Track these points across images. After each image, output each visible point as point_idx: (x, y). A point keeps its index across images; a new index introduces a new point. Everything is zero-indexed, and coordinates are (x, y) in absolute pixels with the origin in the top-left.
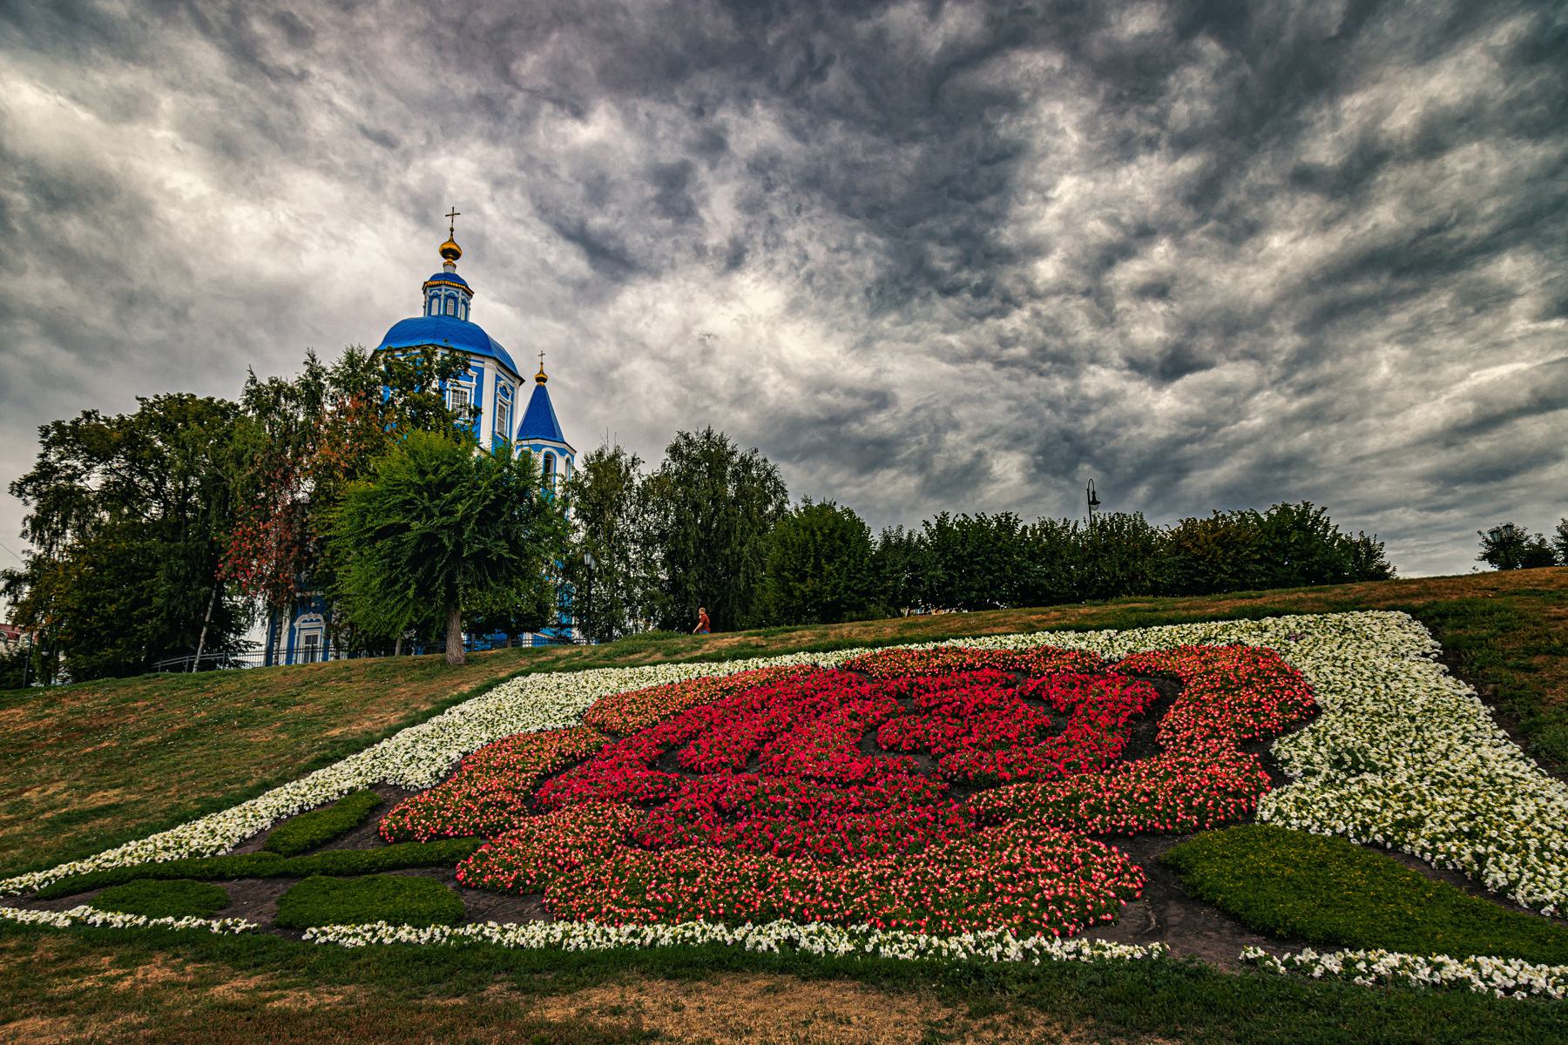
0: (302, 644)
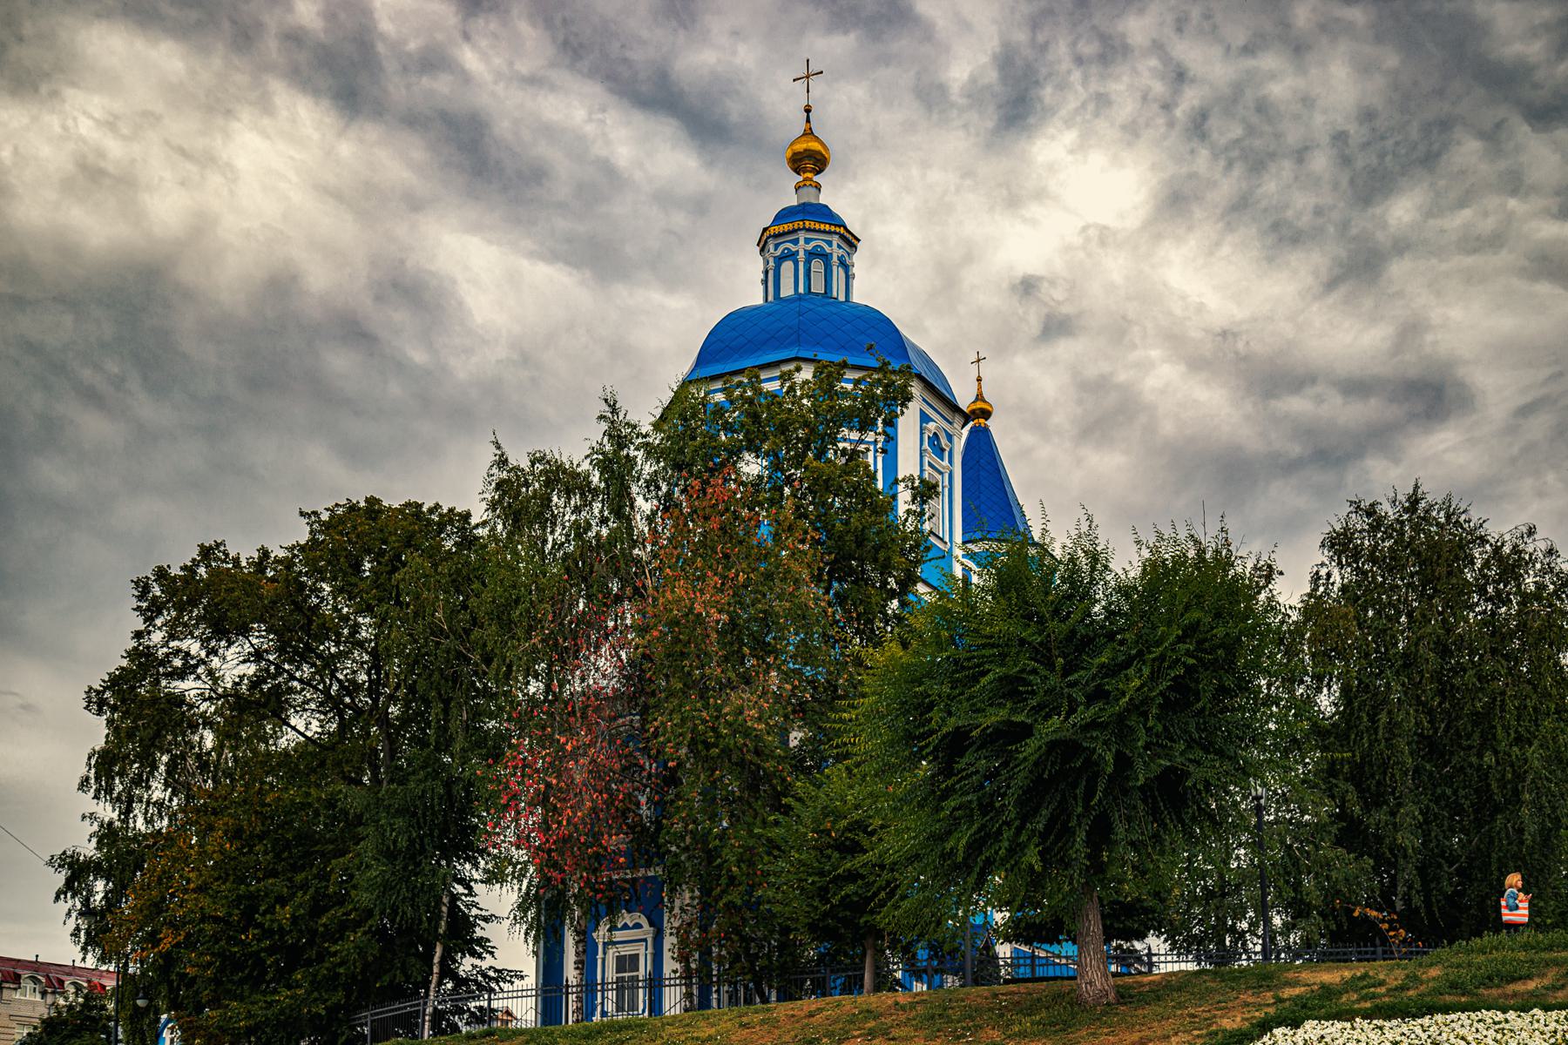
0: (611, 975)
